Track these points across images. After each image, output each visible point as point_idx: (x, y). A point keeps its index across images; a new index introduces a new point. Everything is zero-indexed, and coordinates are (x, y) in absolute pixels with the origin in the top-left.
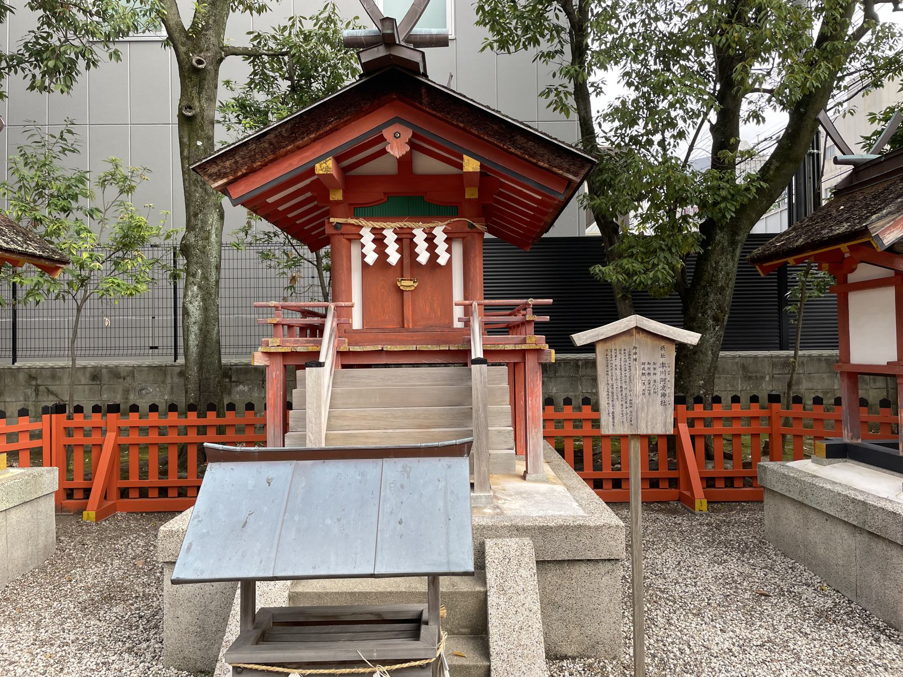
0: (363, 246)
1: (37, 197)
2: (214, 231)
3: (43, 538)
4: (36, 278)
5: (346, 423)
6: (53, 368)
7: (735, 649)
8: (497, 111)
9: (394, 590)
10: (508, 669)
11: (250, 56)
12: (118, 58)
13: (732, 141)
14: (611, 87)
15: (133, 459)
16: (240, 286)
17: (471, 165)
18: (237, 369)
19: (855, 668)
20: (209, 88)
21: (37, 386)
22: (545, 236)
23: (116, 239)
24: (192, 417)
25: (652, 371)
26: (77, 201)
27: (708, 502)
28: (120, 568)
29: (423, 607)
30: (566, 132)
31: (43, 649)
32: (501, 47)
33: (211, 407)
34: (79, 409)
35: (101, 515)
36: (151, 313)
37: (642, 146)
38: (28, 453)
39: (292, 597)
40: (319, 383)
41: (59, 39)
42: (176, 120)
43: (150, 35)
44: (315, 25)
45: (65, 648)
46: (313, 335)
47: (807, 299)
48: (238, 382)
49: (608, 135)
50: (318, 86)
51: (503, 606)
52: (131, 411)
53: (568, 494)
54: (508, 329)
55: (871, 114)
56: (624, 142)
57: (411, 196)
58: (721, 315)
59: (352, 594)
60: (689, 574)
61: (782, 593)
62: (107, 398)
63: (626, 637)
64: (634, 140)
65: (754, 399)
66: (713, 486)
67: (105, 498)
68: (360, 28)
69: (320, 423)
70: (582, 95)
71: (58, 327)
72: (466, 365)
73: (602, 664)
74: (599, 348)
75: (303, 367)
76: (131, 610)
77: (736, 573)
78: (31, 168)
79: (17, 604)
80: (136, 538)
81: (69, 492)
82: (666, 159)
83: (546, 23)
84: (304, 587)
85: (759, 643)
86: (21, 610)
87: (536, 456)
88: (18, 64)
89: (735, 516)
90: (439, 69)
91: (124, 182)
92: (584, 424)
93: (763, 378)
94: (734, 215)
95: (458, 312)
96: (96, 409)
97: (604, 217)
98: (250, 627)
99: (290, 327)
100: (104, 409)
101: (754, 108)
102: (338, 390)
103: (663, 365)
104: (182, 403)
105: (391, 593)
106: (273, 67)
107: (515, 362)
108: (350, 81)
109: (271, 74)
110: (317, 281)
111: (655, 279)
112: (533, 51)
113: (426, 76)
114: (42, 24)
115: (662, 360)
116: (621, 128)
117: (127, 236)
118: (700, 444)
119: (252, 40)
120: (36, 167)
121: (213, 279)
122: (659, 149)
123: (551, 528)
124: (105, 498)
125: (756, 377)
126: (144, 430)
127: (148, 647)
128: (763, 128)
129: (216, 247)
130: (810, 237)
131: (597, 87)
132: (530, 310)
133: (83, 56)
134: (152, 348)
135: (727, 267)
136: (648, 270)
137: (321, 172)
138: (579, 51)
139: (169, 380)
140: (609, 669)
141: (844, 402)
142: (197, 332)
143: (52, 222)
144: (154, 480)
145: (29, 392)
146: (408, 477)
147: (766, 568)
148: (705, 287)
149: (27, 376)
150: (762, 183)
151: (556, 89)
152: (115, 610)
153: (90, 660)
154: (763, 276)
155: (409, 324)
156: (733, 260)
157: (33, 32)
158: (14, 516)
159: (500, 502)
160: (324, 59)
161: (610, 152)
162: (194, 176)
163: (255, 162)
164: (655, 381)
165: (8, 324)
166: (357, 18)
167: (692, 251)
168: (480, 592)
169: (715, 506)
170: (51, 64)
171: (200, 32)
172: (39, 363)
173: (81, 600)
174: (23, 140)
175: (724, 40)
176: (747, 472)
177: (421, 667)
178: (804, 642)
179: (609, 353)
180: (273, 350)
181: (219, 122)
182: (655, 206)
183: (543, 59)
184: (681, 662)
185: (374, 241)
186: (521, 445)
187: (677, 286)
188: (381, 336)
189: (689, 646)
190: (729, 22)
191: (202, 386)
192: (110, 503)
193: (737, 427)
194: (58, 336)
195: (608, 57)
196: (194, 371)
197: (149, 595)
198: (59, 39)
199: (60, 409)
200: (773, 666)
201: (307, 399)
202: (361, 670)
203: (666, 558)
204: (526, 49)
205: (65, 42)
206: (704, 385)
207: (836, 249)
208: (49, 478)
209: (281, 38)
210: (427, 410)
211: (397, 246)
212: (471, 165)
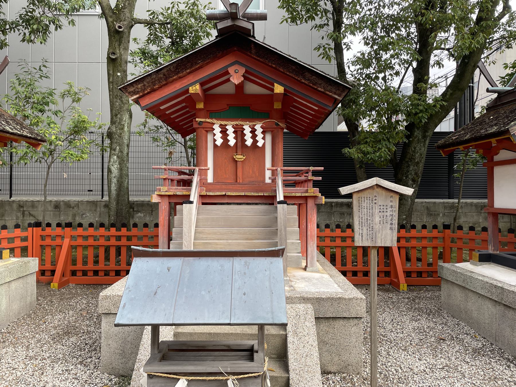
0: (214, 135)
1: (25, 103)
2: (126, 125)
3: (29, 298)
4: (25, 150)
5: (204, 236)
6: (33, 201)
7: (427, 370)
8: (295, 58)
9: (234, 332)
10: (300, 379)
11: (148, 24)
12: (74, 24)
13: (426, 77)
14: (356, 45)
15: (79, 254)
16: (135, 156)
17: (279, 89)
18: (137, 204)
19: (497, 383)
20: (125, 42)
21: (24, 211)
22: (316, 131)
23: (70, 128)
24: (113, 231)
25: (385, 210)
26: (48, 106)
27: (408, 286)
28: (73, 316)
29: (254, 343)
30: (330, 70)
31: (32, 362)
32: (293, 21)
33: (124, 225)
34: (49, 225)
35: (61, 285)
36: (89, 171)
37: (372, 80)
38: (19, 249)
39: (176, 335)
40: (190, 212)
41: (39, 13)
42: (106, 61)
43: (91, 12)
44: (186, 7)
45: (44, 361)
46: (184, 185)
47: (466, 170)
48: (138, 211)
49: (354, 73)
50: (187, 42)
51: (296, 343)
52: (100, 227)
53: (331, 279)
54: (295, 184)
55: (505, 64)
56: (362, 77)
57: (242, 107)
58: (416, 178)
59: (210, 334)
60: (399, 327)
61: (452, 339)
62: (64, 219)
63: (364, 362)
64: (368, 76)
65: (435, 227)
66: (410, 276)
67: (63, 276)
68: (212, 9)
69: (191, 236)
70: (339, 50)
71: (33, 178)
72: (273, 204)
73: (351, 377)
74: (355, 196)
75: (182, 204)
76: (80, 340)
77: (426, 327)
78: (22, 86)
79: (15, 335)
80: (81, 299)
81: (42, 272)
82: (387, 88)
83: (318, 8)
84: (181, 329)
85: (441, 367)
86: (17, 339)
87: (312, 258)
88: (16, 27)
89: (423, 294)
90: (263, 34)
91: (75, 95)
92: (326, 239)
93: (438, 215)
94: (426, 120)
95: (268, 174)
96: (59, 225)
97: (350, 120)
98: (156, 352)
99: (172, 180)
100: (63, 224)
101: (437, 59)
102: (200, 217)
103: (392, 207)
104: (106, 223)
105: (232, 334)
106: (161, 31)
107: (301, 202)
108: (205, 41)
109: (160, 35)
110: (184, 154)
111: (380, 157)
112: (311, 23)
113: (254, 38)
114: (30, 4)
115: (391, 204)
116: (361, 69)
117: (77, 127)
118: (403, 252)
119: (150, 15)
120: (25, 86)
121: (125, 152)
122: (383, 82)
123: (323, 299)
124: (63, 276)
125: (435, 214)
126: (86, 238)
127: (91, 361)
128: (443, 70)
129: (127, 134)
130: (473, 134)
131: (348, 45)
132: (310, 173)
133: (54, 23)
134: (89, 191)
135: (421, 150)
136: (375, 151)
137: (192, 92)
138: (338, 24)
139: (98, 209)
140: (355, 380)
141: (490, 230)
142: (116, 182)
143: (34, 118)
144: (90, 266)
145: (19, 214)
146: (248, 268)
147: (442, 324)
148: (407, 162)
149: (18, 205)
150: (443, 102)
151: (324, 46)
152: (71, 340)
153: (59, 368)
154: (444, 156)
155: (240, 180)
156: (424, 147)
157: (25, 8)
158: (13, 285)
159: (293, 283)
160: (191, 27)
161: (354, 83)
162: (119, 93)
163: (155, 85)
164: (387, 216)
165: (7, 176)
166: (210, 3)
167: (401, 141)
168: (283, 334)
169: (411, 288)
170: (35, 27)
171: (121, 10)
172: (25, 198)
173: (52, 334)
174: (18, 71)
175: (424, 19)
176: (430, 269)
177: (255, 377)
178: (467, 367)
179: (360, 199)
180: (163, 194)
181: (130, 62)
182: (379, 115)
183: (317, 29)
184: (396, 377)
185: (221, 132)
186: (305, 251)
187: (391, 161)
188: (224, 187)
189: (401, 368)
190: (426, 9)
191: (118, 213)
192: (65, 279)
193: (425, 243)
194: (60, 183)
195: (354, 29)
196: (113, 205)
197: (91, 331)
198: (39, 13)
199: (38, 224)
200: (449, 381)
201: (184, 222)
202: (221, 378)
203: (385, 317)
204: (307, 23)
205: (43, 14)
206: (406, 218)
207: (486, 142)
208: (33, 264)
209: (166, 14)
210: (250, 230)
211: (251, 135)
212: (279, 89)
